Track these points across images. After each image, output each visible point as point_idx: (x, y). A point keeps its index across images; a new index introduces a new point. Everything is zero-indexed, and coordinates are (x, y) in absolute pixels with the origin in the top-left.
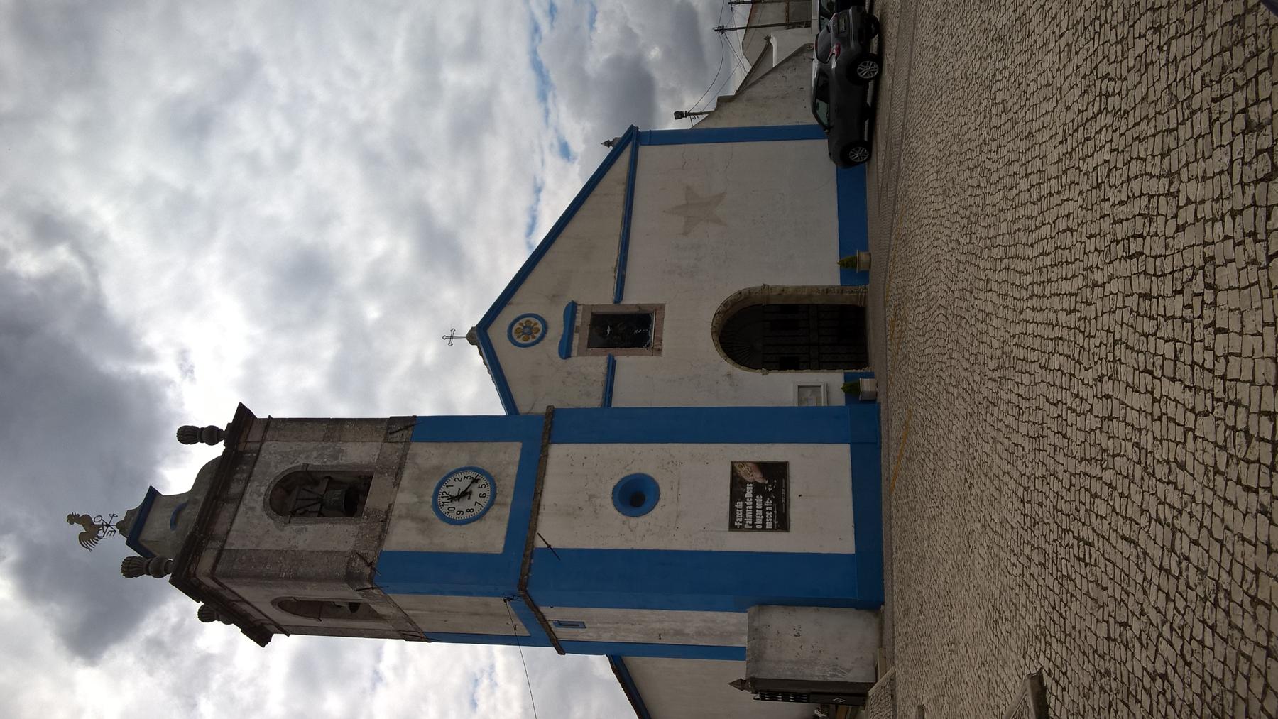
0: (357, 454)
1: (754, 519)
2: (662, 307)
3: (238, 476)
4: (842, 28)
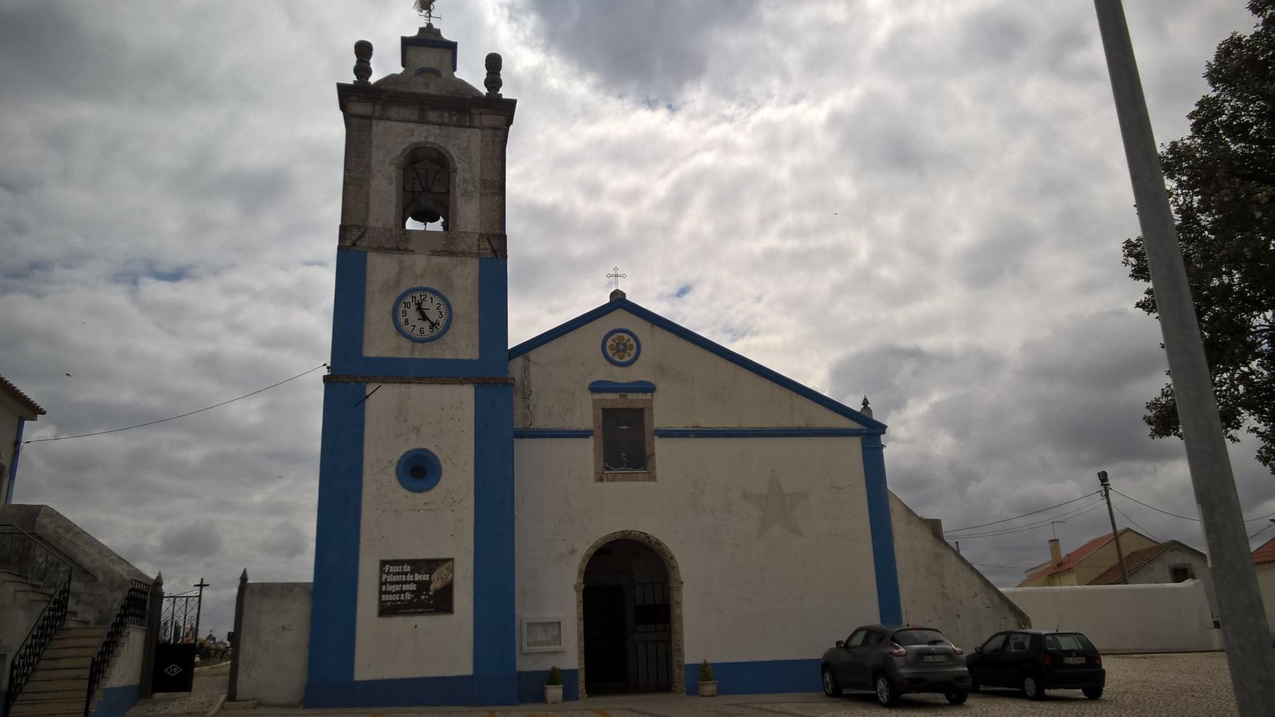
0: (469, 213)
1: (392, 583)
2: (652, 477)
3: (446, 115)
4: (930, 658)
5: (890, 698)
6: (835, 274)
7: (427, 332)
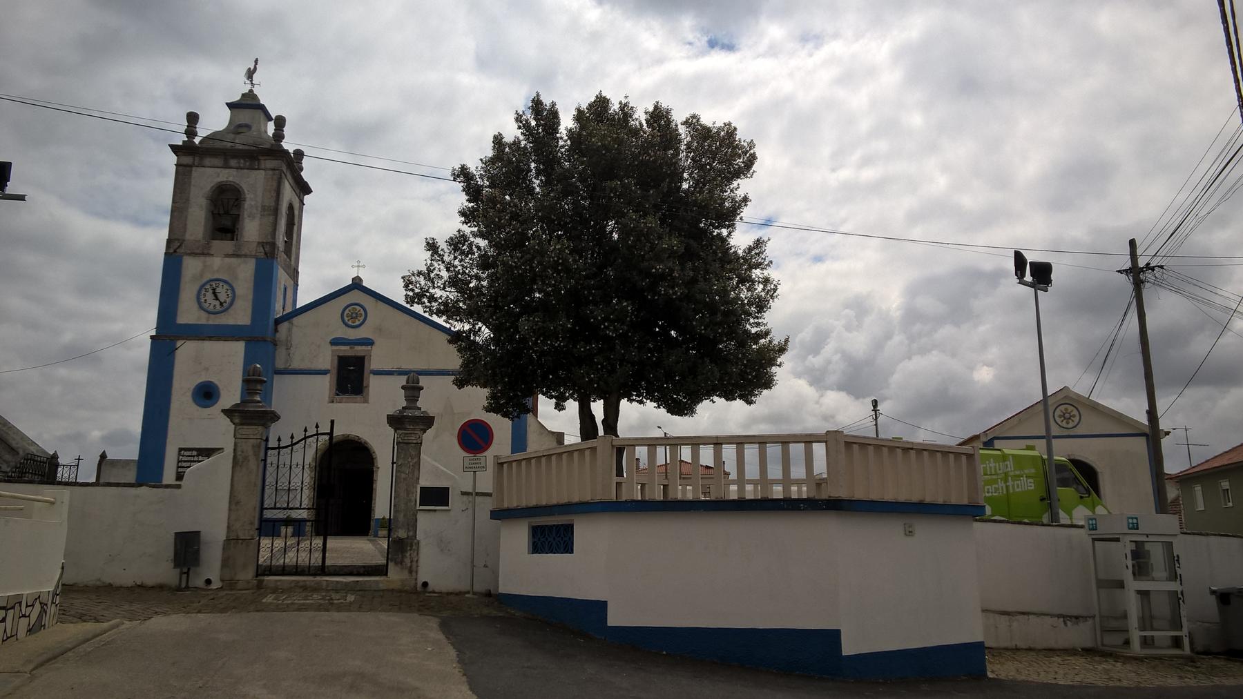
2: (366, 401)
5: (268, 520)
6: (908, 202)
7: (218, 308)
